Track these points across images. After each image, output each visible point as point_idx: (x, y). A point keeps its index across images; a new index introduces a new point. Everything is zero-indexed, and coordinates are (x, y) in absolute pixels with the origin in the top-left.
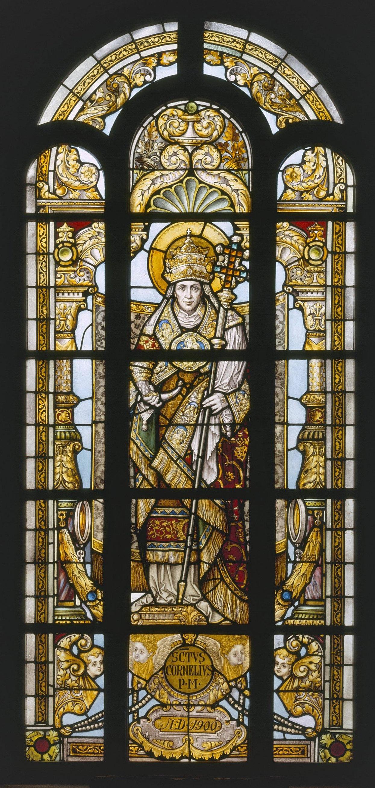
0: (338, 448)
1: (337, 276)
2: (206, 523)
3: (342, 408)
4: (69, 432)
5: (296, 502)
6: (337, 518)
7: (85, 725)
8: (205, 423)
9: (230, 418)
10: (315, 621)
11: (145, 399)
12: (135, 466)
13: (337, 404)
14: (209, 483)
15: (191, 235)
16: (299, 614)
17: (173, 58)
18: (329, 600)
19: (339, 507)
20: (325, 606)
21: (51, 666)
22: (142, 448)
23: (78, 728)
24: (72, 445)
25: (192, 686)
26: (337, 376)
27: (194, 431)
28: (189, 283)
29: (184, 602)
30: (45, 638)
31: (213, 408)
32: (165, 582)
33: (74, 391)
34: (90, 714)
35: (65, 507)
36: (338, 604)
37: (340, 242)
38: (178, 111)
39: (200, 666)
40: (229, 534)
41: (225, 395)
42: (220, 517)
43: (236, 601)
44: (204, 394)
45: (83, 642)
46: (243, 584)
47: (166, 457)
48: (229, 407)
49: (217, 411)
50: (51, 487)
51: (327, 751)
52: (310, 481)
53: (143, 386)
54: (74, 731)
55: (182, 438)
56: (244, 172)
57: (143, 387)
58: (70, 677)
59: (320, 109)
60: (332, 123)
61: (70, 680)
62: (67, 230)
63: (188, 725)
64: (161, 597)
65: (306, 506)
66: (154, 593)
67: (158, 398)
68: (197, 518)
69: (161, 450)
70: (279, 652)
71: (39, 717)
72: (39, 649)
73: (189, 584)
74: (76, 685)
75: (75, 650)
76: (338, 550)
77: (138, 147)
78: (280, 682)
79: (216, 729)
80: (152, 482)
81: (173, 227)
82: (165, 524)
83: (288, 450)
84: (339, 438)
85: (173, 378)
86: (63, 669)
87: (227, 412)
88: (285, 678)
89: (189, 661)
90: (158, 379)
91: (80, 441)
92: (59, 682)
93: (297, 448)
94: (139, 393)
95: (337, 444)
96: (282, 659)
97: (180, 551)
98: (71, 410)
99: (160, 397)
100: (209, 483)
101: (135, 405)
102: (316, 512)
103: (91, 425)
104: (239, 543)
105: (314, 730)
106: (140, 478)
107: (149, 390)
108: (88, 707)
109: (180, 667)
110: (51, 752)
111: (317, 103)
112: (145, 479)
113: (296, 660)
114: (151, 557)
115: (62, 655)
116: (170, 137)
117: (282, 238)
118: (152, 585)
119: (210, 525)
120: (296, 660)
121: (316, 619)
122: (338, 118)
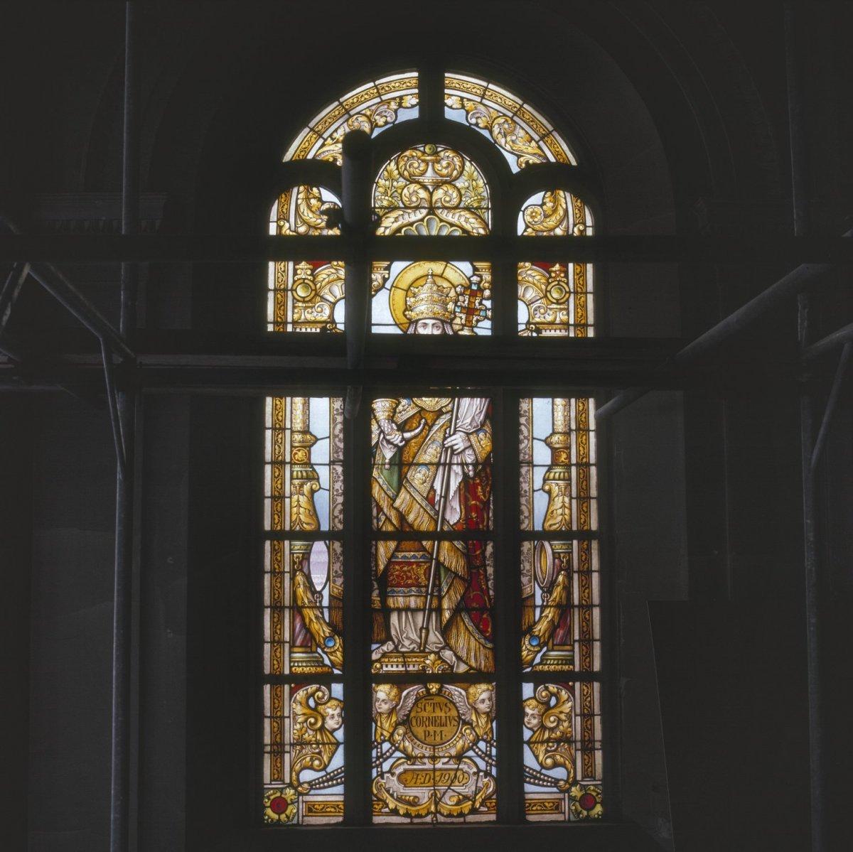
0: (582, 452)
1: (582, 303)
2: (448, 570)
3: (586, 481)
4: (306, 471)
5: (543, 546)
6: (583, 558)
7: (323, 782)
8: (448, 462)
9: (473, 458)
10: (564, 667)
11: (388, 437)
12: (378, 506)
13: (582, 476)
14: (452, 523)
15: (433, 275)
16: (547, 660)
17: (415, 101)
18: (577, 645)
19: (585, 546)
20: (573, 651)
21: (287, 721)
22: (385, 487)
23: (316, 785)
24: (309, 484)
25: (438, 738)
26: (582, 516)
27: (437, 470)
28: (430, 322)
29: (427, 650)
30: (280, 691)
31: (455, 447)
32: (406, 630)
33: (311, 430)
34: (329, 770)
35: (298, 550)
36: (587, 648)
37: (581, 282)
38: (417, 152)
39: (446, 717)
40: (472, 578)
41: (468, 434)
42: (462, 562)
43: (479, 648)
44: (446, 433)
45: (320, 694)
46: (487, 632)
47: (408, 497)
48: (471, 446)
49: (459, 450)
50: (287, 528)
51: (577, 804)
52: (556, 523)
53: (386, 425)
54: (312, 788)
55: (424, 478)
56: (483, 211)
57: (386, 426)
58: (306, 731)
59: (558, 152)
60: (569, 165)
61: (307, 734)
62: (306, 267)
63: (434, 779)
64: (403, 645)
65: (552, 550)
66: (396, 641)
67: (401, 437)
68: (439, 564)
69: (403, 490)
70: (528, 702)
71: (274, 775)
72: (274, 703)
73: (431, 632)
74: (314, 739)
75: (311, 703)
76: (585, 584)
77: (564, 479)
78: (531, 733)
79: (463, 782)
80: (395, 522)
81: (414, 267)
82: (405, 569)
83: (534, 491)
84: (582, 443)
85: (416, 417)
86: (299, 723)
87: (469, 452)
88: (535, 729)
89: (434, 711)
90: (401, 418)
91: (318, 479)
92: (295, 737)
93: (542, 489)
94: (382, 432)
95: (581, 448)
96: (531, 710)
97: (422, 596)
98: (308, 449)
99: (403, 436)
100: (452, 523)
101: (377, 443)
102: (562, 555)
103: (329, 465)
104: (482, 590)
105: (566, 781)
106: (383, 518)
107: (392, 428)
108: (327, 763)
109: (425, 719)
110: (288, 812)
111: (556, 146)
112: (388, 519)
113: (546, 710)
114: (391, 602)
115: (299, 709)
116: (410, 177)
117: (524, 278)
118: (393, 632)
119: (451, 571)
120: (546, 710)
121: (565, 664)
122: (574, 163)
